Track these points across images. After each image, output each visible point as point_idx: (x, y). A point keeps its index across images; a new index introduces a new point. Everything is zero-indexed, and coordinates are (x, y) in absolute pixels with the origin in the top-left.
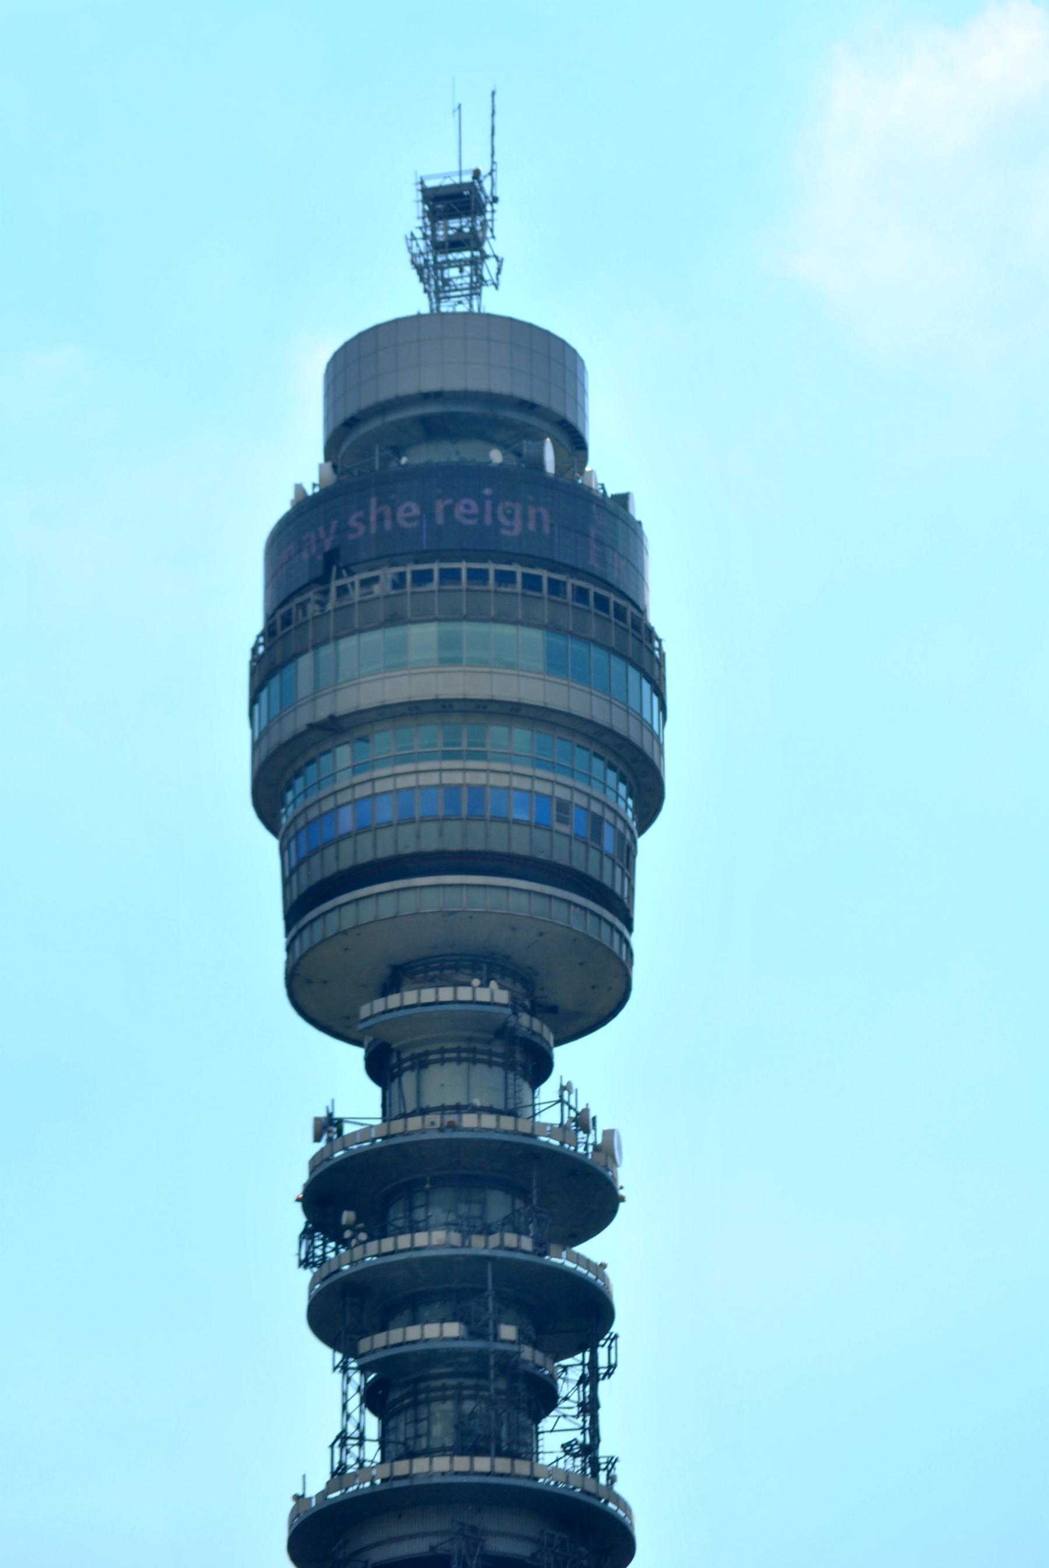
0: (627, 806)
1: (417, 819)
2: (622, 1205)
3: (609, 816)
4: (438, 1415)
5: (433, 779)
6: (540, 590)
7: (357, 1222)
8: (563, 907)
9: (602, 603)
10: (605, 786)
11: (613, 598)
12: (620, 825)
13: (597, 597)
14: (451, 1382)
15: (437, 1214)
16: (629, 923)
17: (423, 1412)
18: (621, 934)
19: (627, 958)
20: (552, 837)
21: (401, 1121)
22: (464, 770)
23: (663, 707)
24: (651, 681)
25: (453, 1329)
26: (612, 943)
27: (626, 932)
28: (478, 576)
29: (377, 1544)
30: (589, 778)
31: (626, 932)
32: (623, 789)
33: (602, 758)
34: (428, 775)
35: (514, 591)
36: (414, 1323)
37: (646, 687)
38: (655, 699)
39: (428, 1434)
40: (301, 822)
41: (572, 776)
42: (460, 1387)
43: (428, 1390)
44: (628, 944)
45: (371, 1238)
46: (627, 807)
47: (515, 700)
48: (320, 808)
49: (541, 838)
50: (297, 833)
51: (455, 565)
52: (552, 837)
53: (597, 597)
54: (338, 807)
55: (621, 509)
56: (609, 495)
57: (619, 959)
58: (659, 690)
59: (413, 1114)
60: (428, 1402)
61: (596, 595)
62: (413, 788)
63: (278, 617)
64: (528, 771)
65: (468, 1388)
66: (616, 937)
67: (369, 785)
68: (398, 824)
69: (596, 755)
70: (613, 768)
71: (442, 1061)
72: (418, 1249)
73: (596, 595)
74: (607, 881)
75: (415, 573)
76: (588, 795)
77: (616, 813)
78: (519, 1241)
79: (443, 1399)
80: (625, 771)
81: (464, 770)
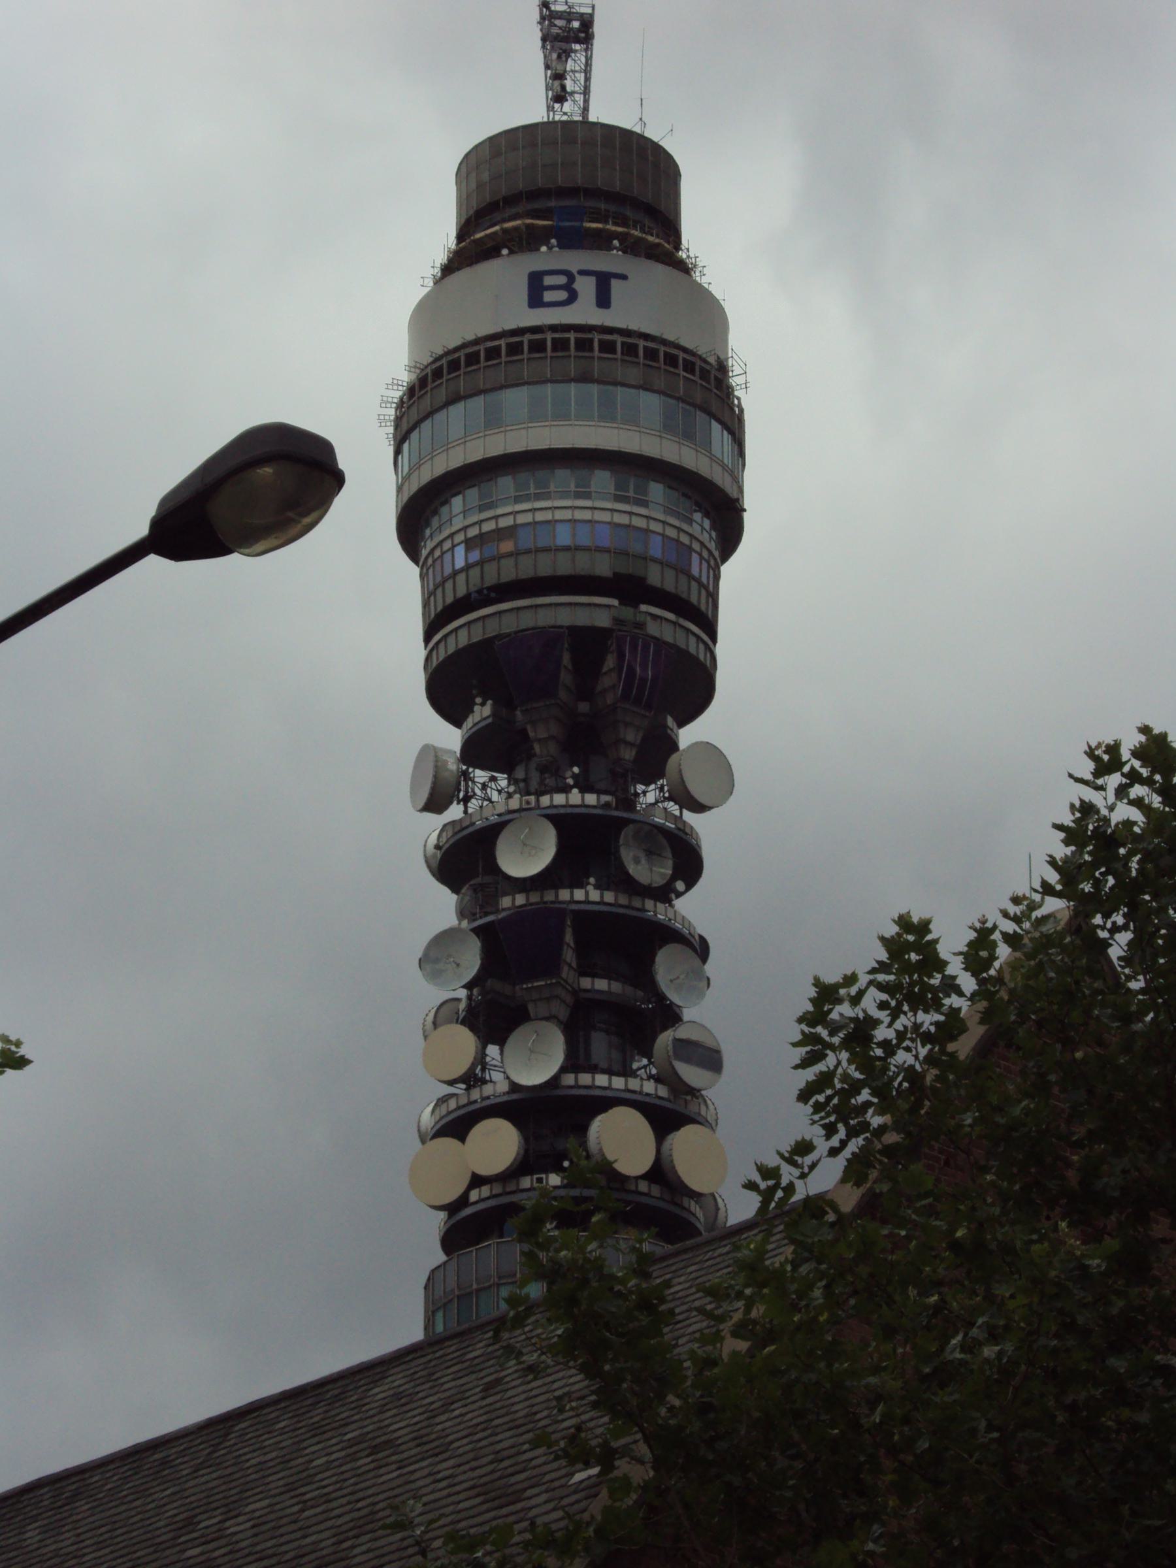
3: (696, 546)
16: (713, 637)
27: (710, 643)
31: (710, 643)
32: (707, 523)
50: (454, 546)
73: (666, 354)
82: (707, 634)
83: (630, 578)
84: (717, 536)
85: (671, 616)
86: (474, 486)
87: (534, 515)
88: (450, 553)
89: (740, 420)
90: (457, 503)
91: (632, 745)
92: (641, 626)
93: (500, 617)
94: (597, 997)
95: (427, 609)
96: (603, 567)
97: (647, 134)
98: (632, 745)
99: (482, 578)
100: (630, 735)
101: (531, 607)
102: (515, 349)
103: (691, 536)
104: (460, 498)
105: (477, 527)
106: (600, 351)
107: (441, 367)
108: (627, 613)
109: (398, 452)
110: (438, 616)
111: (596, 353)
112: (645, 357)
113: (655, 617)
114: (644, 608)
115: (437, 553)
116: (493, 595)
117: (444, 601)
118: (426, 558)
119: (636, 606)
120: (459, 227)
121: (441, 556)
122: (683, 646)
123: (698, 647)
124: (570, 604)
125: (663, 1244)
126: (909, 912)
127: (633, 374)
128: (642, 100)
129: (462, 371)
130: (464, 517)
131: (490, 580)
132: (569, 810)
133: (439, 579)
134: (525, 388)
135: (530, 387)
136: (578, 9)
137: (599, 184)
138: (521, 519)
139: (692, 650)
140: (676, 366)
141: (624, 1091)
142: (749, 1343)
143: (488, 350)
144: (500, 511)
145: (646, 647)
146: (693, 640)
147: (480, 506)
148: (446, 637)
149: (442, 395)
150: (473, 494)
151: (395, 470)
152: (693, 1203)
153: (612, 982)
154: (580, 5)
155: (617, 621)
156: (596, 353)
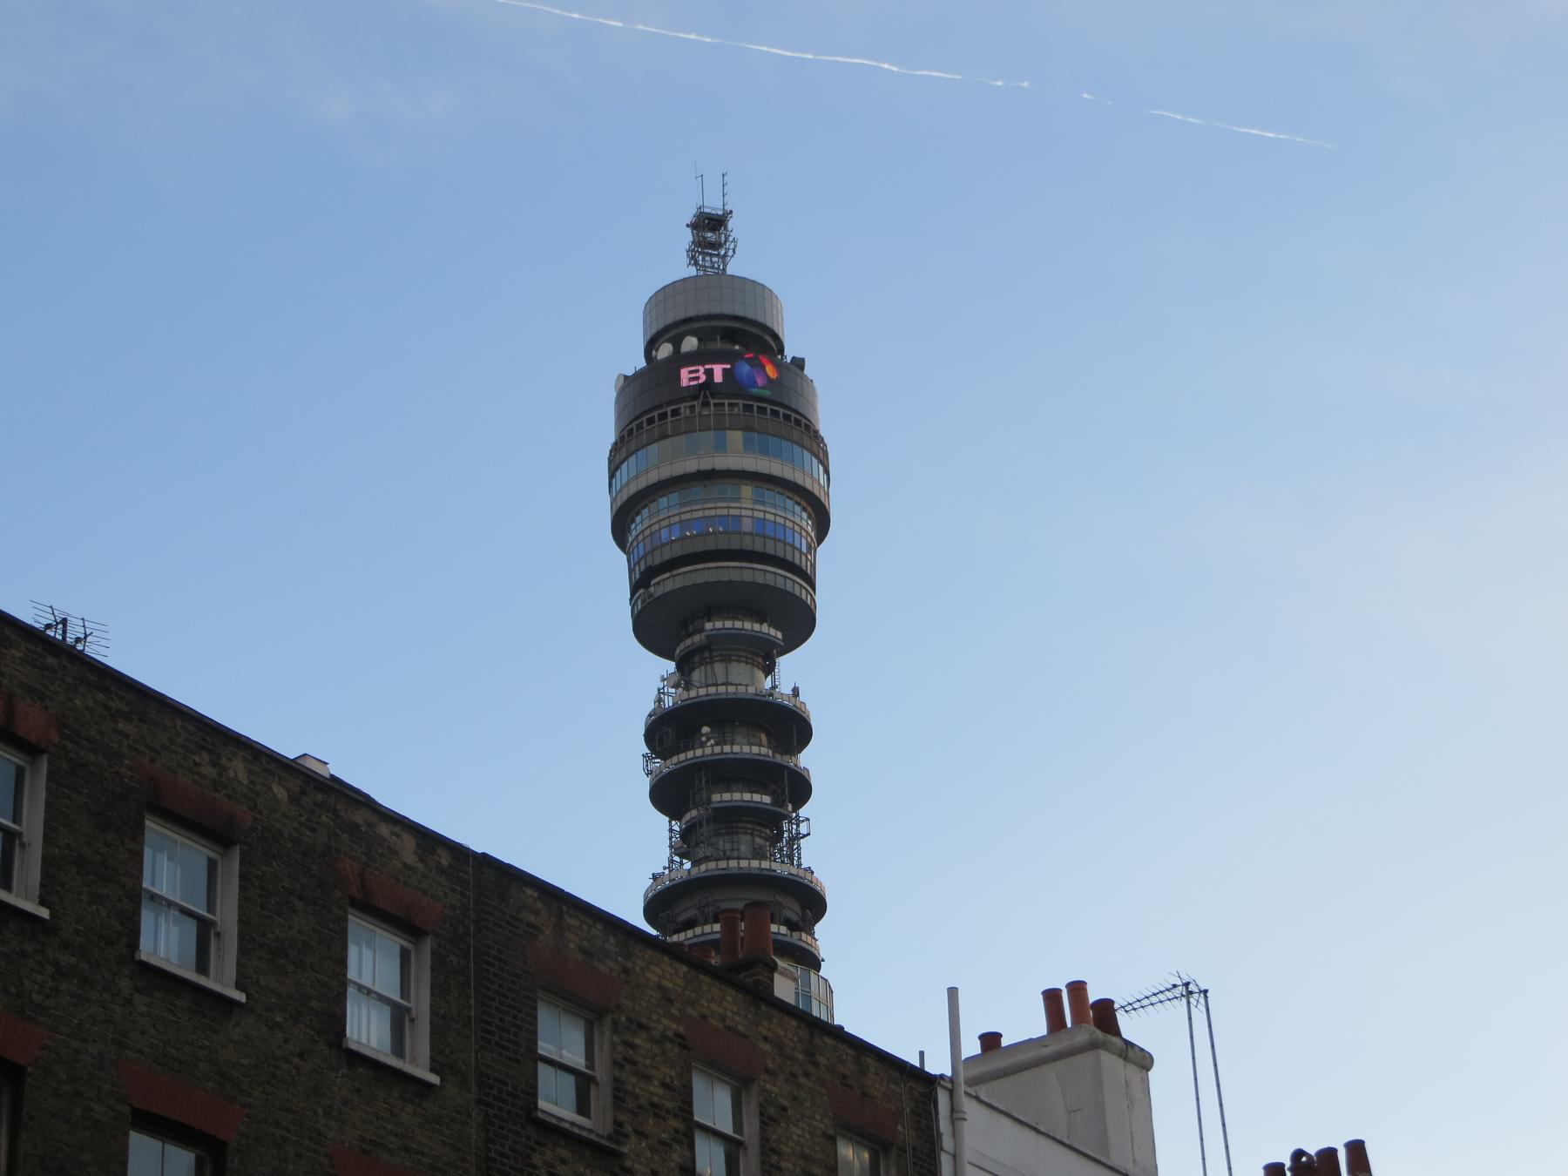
0: (808, 524)
4: (743, 841)
6: (753, 412)
7: (711, 733)
8: (762, 573)
9: (787, 417)
10: (801, 518)
11: (793, 415)
12: (809, 539)
13: (784, 415)
14: (750, 826)
15: (738, 738)
16: (813, 587)
17: (736, 838)
18: (811, 596)
20: (765, 541)
21: (724, 687)
22: (715, 508)
23: (827, 471)
24: (817, 457)
25: (767, 799)
29: (724, 900)
30: (785, 509)
31: (812, 593)
33: (792, 499)
36: (728, 791)
39: (738, 850)
40: (647, 532)
41: (775, 508)
42: (753, 829)
43: (737, 828)
44: (814, 601)
45: (716, 744)
46: (808, 526)
47: (741, 469)
49: (759, 541)
51: (737, 401)
52: (765, 541)
53: (784, 415)
54: (660, 529)
55: (799, 371)
57: (811, 609)
59: (722, 685)
60: (737, 833)
61: (783, 413)
63: (625, 432)
64: (750, 506)
65: (750, 829)
66: (809, 597)
69: (789, 498)
70: (799, 504)
71: (739, 661)
72: (725, 753)
74: (797, 562)
76: (784, 517)
77: (801, 528)
79: (746, 834)
80: (805, 505)
81: (715, 508)
82: (808, 584)
84: (813, 523)
85: (667, 575)
86: (664, 496)
88: (649, 537)
89: (826, 454)
90: (663, 501)
101: (739, 567)
102: (640, 427)
103: (794, 522)
104: (665, 499)
105: (658, 524)
107: (632, 429)
109: (612, 476)
110: (637, 582)
112: (758, 412)
115: (635, 544)
118: (632, 543)
121: (637, 546)
122: (791, 591)
124: (717, 568)
129: (656, 424)
131: (658, 561)
132: (744, 804)
133: (636, 559)
134: (683, 435)
135: (687, 435)
138: (744, 512)
139: (804, 597)
141: (716, 869)
142: (48, 918)
143: (672, 411)
144: (694, 507)
146: (797, 587)
147: (680, 504)
149: (633, 446)
150: (674, 497)
152: (804, 936)
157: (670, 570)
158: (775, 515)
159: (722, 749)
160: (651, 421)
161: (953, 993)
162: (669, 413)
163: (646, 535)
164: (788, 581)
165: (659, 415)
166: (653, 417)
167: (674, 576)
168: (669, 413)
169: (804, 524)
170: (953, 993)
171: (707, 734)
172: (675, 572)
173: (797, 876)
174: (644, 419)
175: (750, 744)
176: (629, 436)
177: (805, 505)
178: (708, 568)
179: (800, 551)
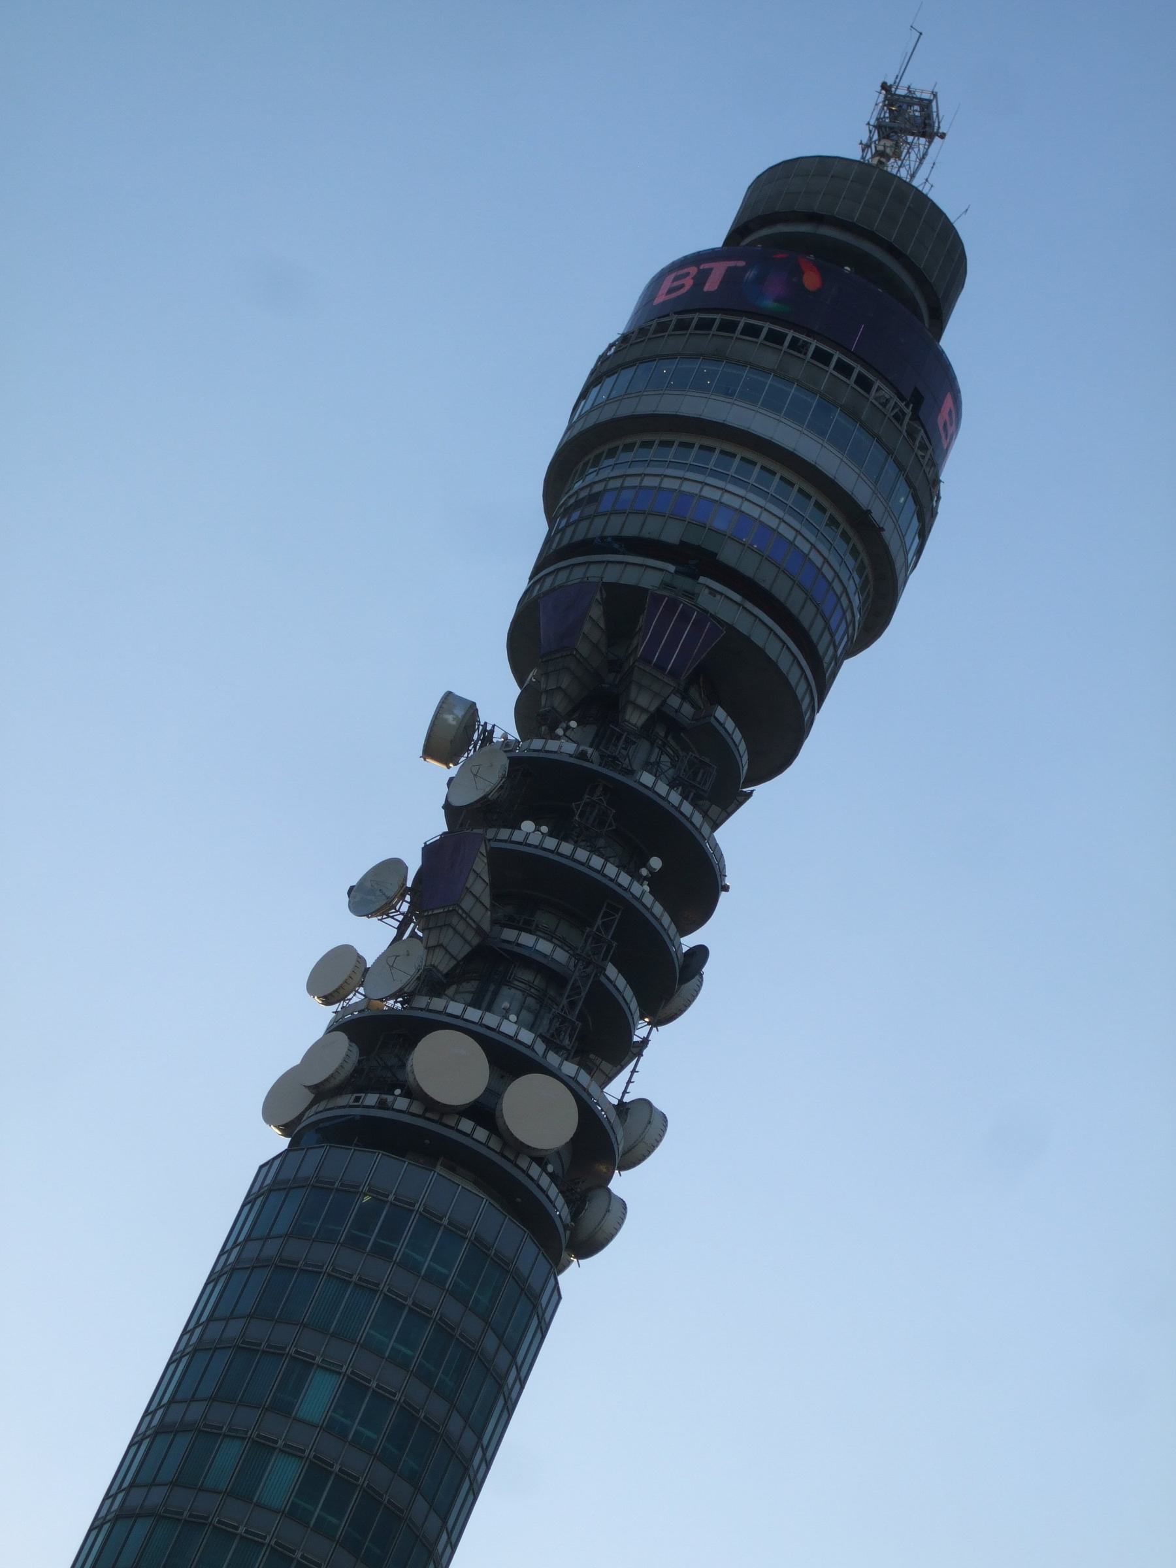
1: (688, 520)
2: (723, 896)
5: (735, 503)
8: (779, 645)
19: (808, 721)
22: (782, 520)
26: (803, 699)
28: (821, 357)
34: (671, 480)
35: (848, 382)
37: (915, 524)
38: (917, 540)
48: (642, 480)
56: (288, 1140)
58: (923, 534)
62: (715, 501)
67: (679, 481)
68: (649, 514)
75: (770, 331)
78: (631, 884)
81: (782, 520)
83: (699, 550)
85: (737, 597)
87: (742, 503)
91: (643, 710)
92: (692, 596)
93: (625, 566)
94: (535, 957)
95: (548, 545)
96: (672, 534)
97: (930, 196)
98: (643, 710)
99: (605, 527)
100: (643, 700)
101: (641, 565)
106: (856, 382)
108: (684, 583)
111: (831, 368)
113: (713, 592)
114: (702, 579)
116: (616, 546)
117: (571, 538)
119: (695, 577)
120: (733, 229)
123: (828, 647)
125: (526, 1230)
126: (309, 1088)
127: (770, 358)
128: (934, 164)
130: (612, 470)
136: (918, 95)
137: (875, 228)
140: (848, 376)
145: (685, 616)
148: (559, 570)
151: (572, 413)
153: (453, 963)
154: (922, 92)
155: (665, 585)
156: (831, 368)
157: (746, 596)
158: (826, 560)
159: (558, 845)
160: (705, 325)
161: (579, 1266)
162: (764, 332)
163: (626, 484)
164: (795, 666)
165: (746, 325)
166: (760, 329)
167: (744, 608)
168: (764, 332)
169: (851, 588)
170: (579, 1266)
171: (651, 870)
172: (749, 605)
173: (585, 1089)
174: (696, 317)
175: (621, 866)
176: (656, 332)
177: (866, 562)
178: (726, 597)
179: (832, 635)
